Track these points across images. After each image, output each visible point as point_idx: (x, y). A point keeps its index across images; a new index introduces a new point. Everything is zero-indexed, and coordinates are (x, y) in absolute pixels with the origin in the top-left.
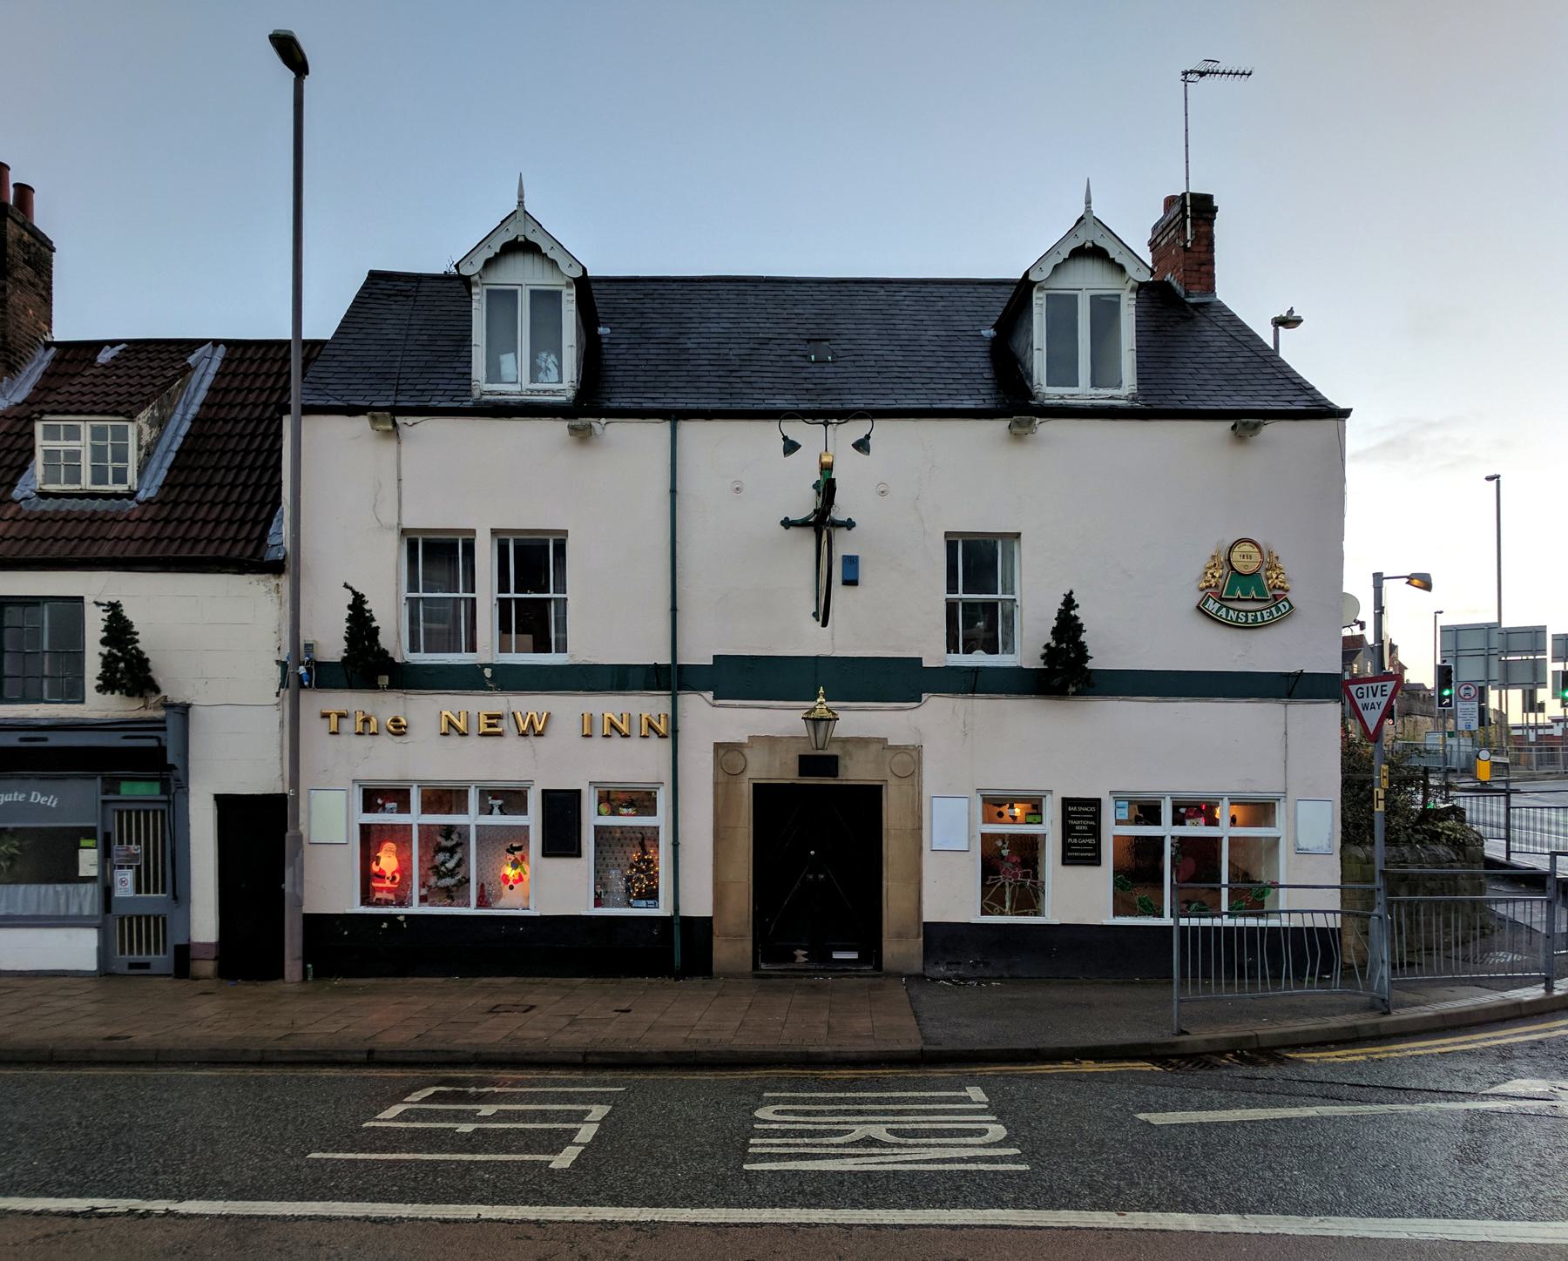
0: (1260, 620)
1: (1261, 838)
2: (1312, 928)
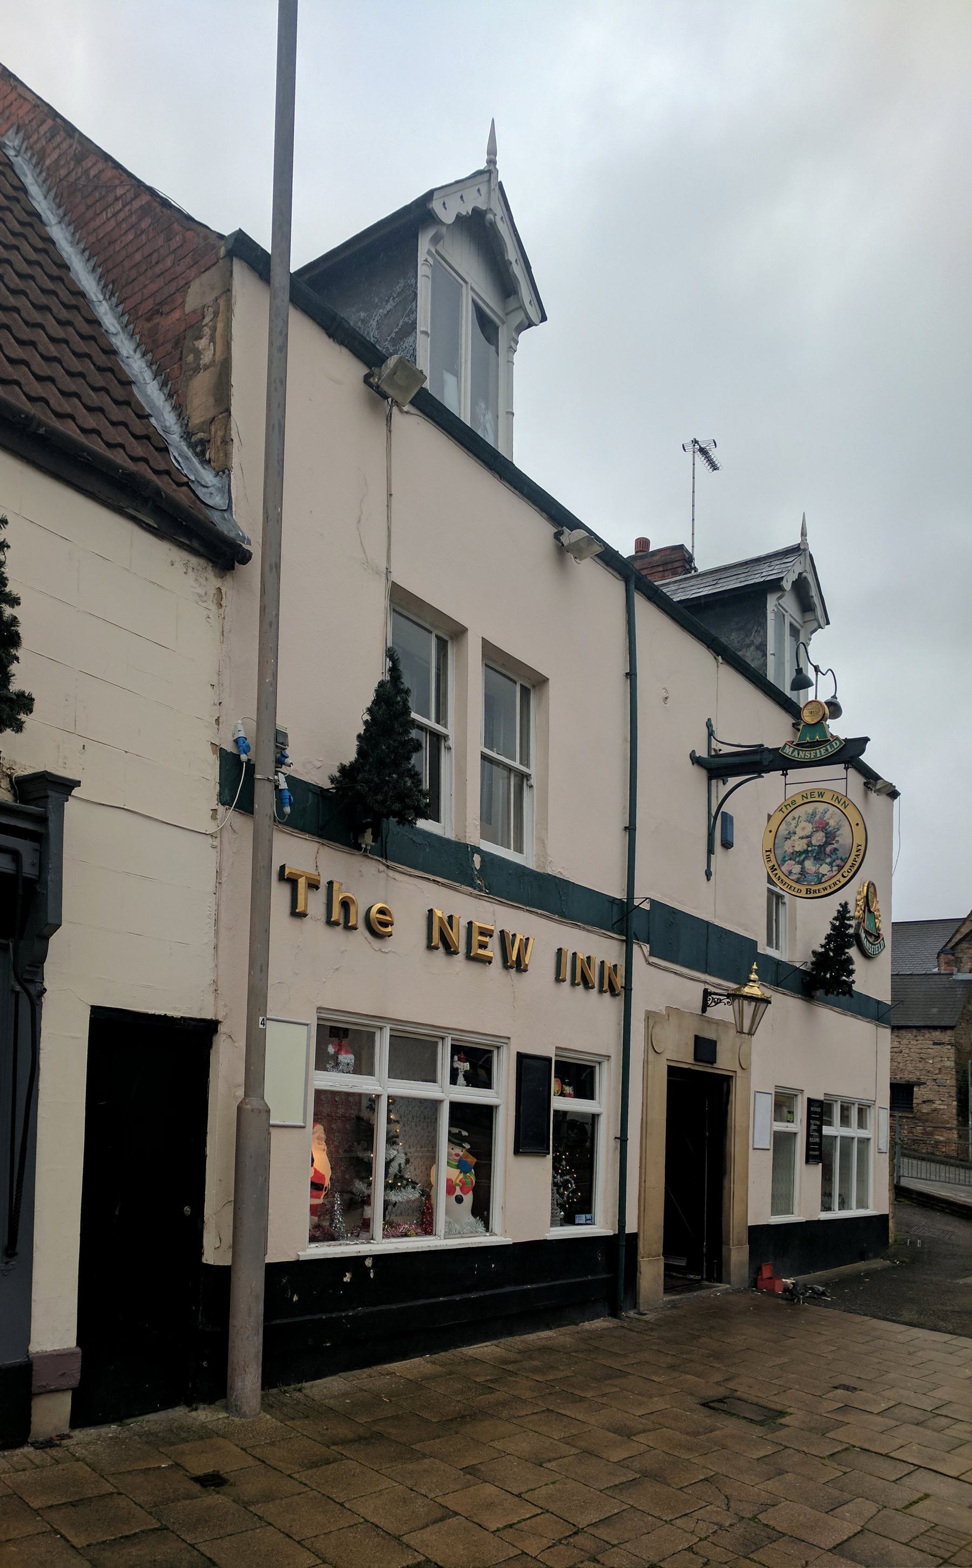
0: (819, 755)
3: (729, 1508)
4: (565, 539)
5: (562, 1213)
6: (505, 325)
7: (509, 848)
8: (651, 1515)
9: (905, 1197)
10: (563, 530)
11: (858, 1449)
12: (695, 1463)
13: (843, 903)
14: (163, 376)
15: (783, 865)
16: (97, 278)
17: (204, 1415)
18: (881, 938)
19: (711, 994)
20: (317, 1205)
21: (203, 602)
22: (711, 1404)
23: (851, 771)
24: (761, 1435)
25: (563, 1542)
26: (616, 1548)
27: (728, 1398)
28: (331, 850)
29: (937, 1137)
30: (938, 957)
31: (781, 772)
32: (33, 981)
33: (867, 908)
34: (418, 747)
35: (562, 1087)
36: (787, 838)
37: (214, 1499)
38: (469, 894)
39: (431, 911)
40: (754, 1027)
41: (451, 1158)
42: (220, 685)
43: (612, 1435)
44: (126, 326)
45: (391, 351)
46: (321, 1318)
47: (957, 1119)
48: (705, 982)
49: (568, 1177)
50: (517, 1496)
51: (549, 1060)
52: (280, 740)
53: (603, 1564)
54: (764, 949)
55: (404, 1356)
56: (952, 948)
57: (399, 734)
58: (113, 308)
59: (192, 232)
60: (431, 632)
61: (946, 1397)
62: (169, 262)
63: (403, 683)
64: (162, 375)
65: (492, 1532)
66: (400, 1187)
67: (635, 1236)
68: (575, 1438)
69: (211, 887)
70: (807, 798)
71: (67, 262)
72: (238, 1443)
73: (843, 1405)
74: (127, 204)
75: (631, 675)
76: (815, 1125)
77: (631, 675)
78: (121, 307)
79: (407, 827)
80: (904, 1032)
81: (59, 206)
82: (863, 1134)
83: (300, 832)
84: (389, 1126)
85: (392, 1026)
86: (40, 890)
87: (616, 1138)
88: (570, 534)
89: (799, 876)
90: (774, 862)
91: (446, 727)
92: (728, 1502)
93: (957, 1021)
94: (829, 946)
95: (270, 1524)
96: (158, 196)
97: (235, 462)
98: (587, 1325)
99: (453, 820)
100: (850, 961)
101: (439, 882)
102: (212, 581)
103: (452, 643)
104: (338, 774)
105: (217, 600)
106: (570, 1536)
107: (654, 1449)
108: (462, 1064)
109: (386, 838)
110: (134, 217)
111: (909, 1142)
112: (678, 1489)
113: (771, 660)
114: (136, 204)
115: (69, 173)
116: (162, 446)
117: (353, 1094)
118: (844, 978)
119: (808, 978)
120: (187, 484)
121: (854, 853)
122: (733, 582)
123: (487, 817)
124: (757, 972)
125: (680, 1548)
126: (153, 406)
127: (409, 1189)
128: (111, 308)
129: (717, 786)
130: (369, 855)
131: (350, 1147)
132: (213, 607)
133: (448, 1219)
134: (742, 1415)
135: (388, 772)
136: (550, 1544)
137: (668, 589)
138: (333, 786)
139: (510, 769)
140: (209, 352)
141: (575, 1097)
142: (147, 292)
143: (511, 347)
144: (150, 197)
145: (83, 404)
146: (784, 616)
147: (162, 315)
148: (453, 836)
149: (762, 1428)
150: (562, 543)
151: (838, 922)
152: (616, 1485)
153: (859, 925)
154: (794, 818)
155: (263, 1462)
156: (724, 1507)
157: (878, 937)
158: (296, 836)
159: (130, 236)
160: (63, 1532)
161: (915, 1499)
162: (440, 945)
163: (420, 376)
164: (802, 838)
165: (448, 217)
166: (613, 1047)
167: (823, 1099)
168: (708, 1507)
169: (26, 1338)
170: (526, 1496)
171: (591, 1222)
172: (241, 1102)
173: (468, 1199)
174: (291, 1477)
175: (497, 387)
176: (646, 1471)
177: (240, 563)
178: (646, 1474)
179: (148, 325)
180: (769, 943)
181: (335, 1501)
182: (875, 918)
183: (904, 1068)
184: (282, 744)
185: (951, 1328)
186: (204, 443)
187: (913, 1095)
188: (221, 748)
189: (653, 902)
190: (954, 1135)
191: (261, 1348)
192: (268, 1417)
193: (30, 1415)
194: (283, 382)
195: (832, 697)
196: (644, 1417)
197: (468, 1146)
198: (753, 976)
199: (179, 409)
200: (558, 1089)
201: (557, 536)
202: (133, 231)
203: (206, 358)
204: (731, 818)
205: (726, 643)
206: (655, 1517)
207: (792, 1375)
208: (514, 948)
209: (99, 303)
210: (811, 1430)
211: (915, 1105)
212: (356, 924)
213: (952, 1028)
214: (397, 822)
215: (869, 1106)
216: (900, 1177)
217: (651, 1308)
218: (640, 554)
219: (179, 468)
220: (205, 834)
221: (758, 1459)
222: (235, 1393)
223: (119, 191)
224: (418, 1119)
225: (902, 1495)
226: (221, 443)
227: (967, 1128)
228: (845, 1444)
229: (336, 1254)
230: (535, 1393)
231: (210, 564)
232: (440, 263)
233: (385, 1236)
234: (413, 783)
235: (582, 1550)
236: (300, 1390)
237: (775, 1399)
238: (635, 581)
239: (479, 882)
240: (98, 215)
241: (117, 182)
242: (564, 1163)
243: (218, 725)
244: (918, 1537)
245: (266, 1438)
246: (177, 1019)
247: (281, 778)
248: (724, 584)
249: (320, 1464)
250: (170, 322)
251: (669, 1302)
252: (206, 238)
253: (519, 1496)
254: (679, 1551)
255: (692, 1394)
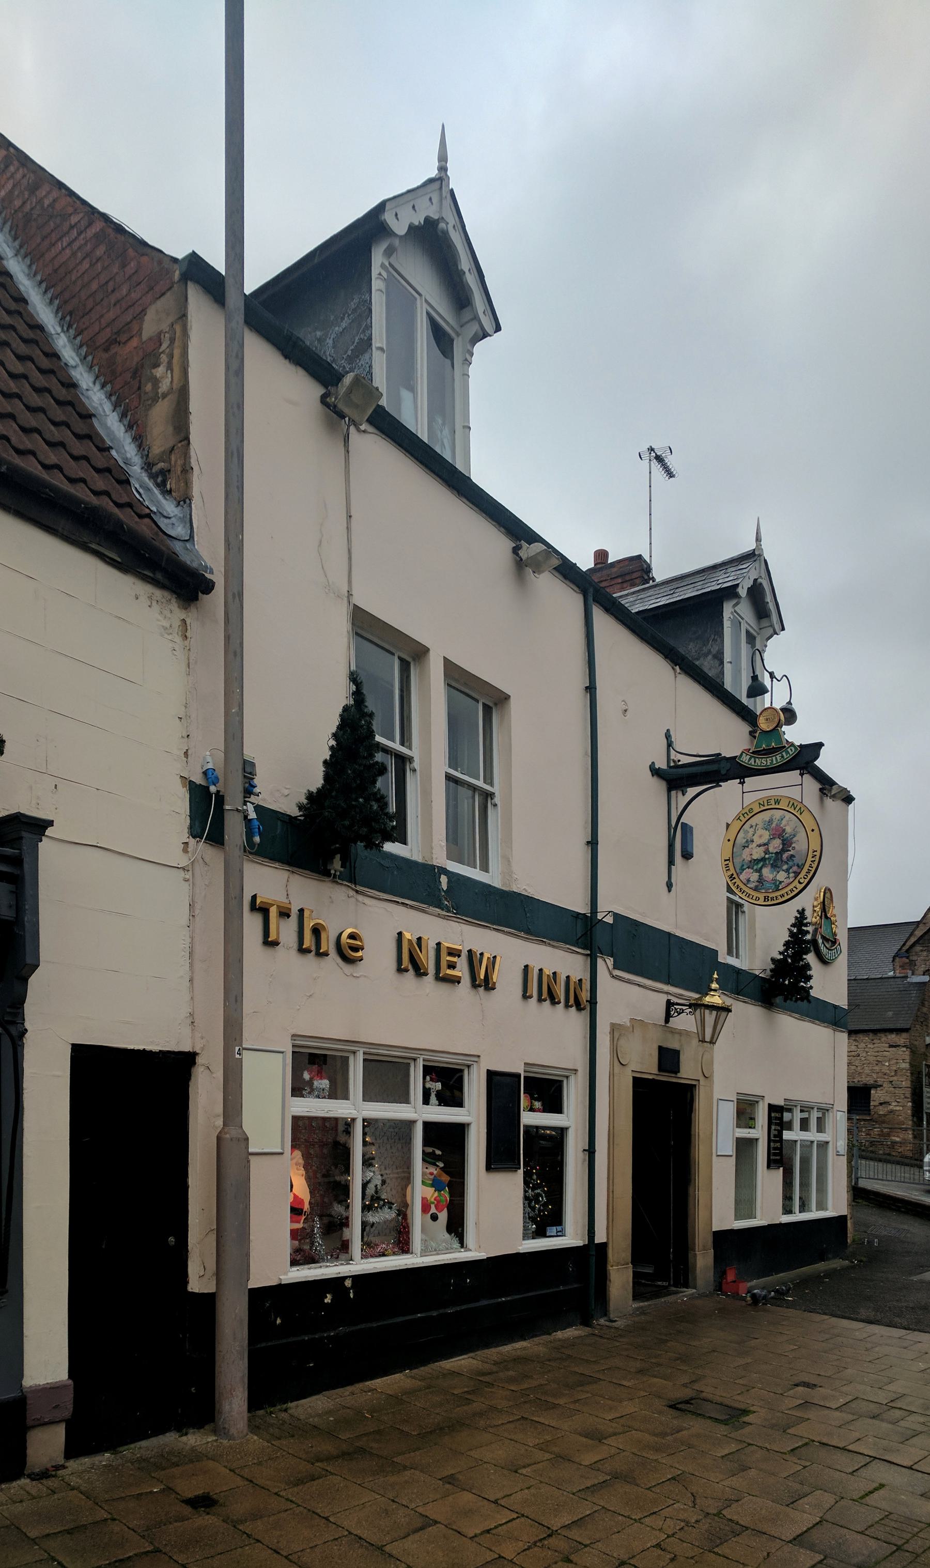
0: (775, 762)
3: (695, 1505)
4: (523, 554)
5: (534, 1226)
6: (460, 338)
7: (475, 868)
8: (622, 1515)
9: (862, 1198)
10: (521, 545)
11: (818, 1444)
12: (663, 1463)
13: (800, 909)
14: (123, 407)
15: (741, 873)
16: (54, 311)
17: (194, 1440)
18: (838, 943)
19: (674, 1004)
20: (298, 1229)
21: (169, 634)
22: (677, 1406)
23: (807, 777)
24: (725, 1433)
25: (538, 1544)
26: (588, 1548)
27: (694, 1399)
28: (303, 878)
29: (893, 1138)
30: (893, 961)
31: (738, 781)
32: (14, 1023)
33: (823, 913)
34: (382, 770)
35: (531, 1103)
36: (744, 847)
37: (206, 1520)
38: (437, 915)
39: (400, 934)
40: (716, 1036)
41: (426, 1177)
42: (188, 717)
43: (584, 1440)
44: (85, 358)
45: (347, 369)
46: (304, 1340)
47: (913, 1120)
48: (667, 993)
49: (539, 1191)
50: (494, 1503)
51: (518, 1076)
52: (248, 769)
53: (576, 1564)
54: (725, 959)
55: (386, 1373)
56: (907, 951)
57: (365, 758)
58: (72, 340)
59: (146, 257)
60: (393, 654)
61: (900, 1390)
62: (125, 290)
63: (366, 707)
64: (121, 406)
65: (471, 1538)
66: (377, 1208)
67: (604, 1246)
68: (548, 1444)
69: (184, 920)
70: (764, 806)
71: (25, 295)
72: (226, 1464)
73: (803, 1402)
74: (81, 232)
75: (591, 689)
76: (775, 1130)
77: (591, 689)
78: (79, 339)
79: (374, 851)
80: (861, 1036)
81: (15, 239)
82: (821, 1137)
83: (271, 861)
84: (365, 1149)
85: (365, 1050)
86: (17, 932)
87: (584, 1150)
88: (528, 548)
89: (758, 884)
90: (732, 871)
91: (410, 749)
92: (695, 1499)
93: (912, 1024)
94: (788, 953)
95: (258, 1541)
96: (112, 222)
97: (196, 491)
98: (559, 1334)
99: (420, 842)
100: (808, 967)
101: (407, 905)
102: (175, 613)
103: (415, 665)
104: (305, 801)
105: (182, 632)
106: (544, 1538)
107: (624, 1451)
108: (434, 1084)
109: (355, 863)
110: (89, 244)
111: (867, 1143)
112: (646, 1489)
113: (728, 668)
114: (90, 232)
115: (24, 203)
116: (124, 478)
117: (330, 1118)
118: (802, 984)
119: (767, 985)
120: (148, 516)
121: (810, 859)
122: (690, 591)
123: (453, 836)
124: (717, 981)
125: (649, 1545)
126: (113, 438)
127: (386, 1209)
128: (69, 341)
129: (677, 797)
130: (339, 881)
131: (328, 1171)
132: (178, 639)
133: (424, 1237)
134: (708, 1415)
135: (354, 796)
136: (526, 1547)
137: (627, 601)
138: (301, 813)
139: (474, 788)
140: (167, 380)
141: (544, 1111)
142: (104, 322)
143: (466, 360)
144: (104, 224)
145: (44, 439)
146: (740, 623)
147: (119, 344)
148: (420, 858)
149: (727, 1427)
150: (520, 557)
151: (796, 929)
152: (588, 1488)
153: (816, 931)
154: (752, 826)
155: (251, 1481)
156: (691, 1504)
157: (834, 942)
158: (266, 865)
159: (86, 265)
160: (60, 1559)
161: (871, 1488)
162: (410, 967)
163: (375, 393)
164: (760, 846)
165: (400, 228)
166: (580, 1062)
167: (783, 1104)
168: (675, 1505)
169: (21, 1375)
170: (502, 1502)
171: (561, 1234)
172: (220, 1132)
173: (443, 1216)
174: (279, 1495)
175: (454, 407)
176: (617, 1472)
177: (203, 593)
178: (616, 1476)
179: (105, 356)
180: (730, 952)
181: (320, 1516)
182: (832, 923)
183: (861, 1071)
184: (250, 773)
185: (906, 1323)
186: (165, 473)
187: (870, 1098)
188: (190, 781)
189: (616, 916)
190: (910, 1136)
191: (246, 1372)
192: (256, 1438)
193: (25, 1448)
194: (240, 406)
195: (787, 703)
196: (614, 1421)
197: (441, 1165)
198: (714, 985)
199: (139, 440)
200: (527, 1104)
201: (515, 551)
202: (88, 260)
203: (164, 386)
204: (691, 829)
205: (684, 653)
206: (625, 1517)
207: (755, 1375)
208: (482, 967)
209: (57, 336)
210: (773, 1427)
211: (872, 1107)
212: (327, 951)
213: (906, 1030)
214: (364, 846)
215: (828, 1110)
216: (857, 1179)
217: (620, 1315)
218: (599, 566)
219: (141, 499)
220: (178, 868)
221: (723, 1457)
222: (223, 1417)
223: (74, 219)
224: (393, 1141)
225: (859, 1485)
226: (182, 472)
227: (920, 1128)
228: (805, 1439)
229: (316, 1276)
230: (510, 1403)
231: (174, 596)
232: (395, 276)
233: (364, 1257)
234: (379, 806)
235: (556, 1551)
236: (286, 1410)
237: (739, 1398)
238: (593, 594)
239: (446, 903)
240: (54, 245)
241: (70, 210)
242: (535, 1177)
243: (187, 758)
244: (872, 1526)
245: (254, 1459)
246: (155, 1053)
247: (250, 808)
248: (681, 593)
249: (305, 1481)
250: (128, 352)
251: (638, 1309)
252: (160, 262)
253: (496, 1502)
254: (648, 1548)
255: (659, 1397)
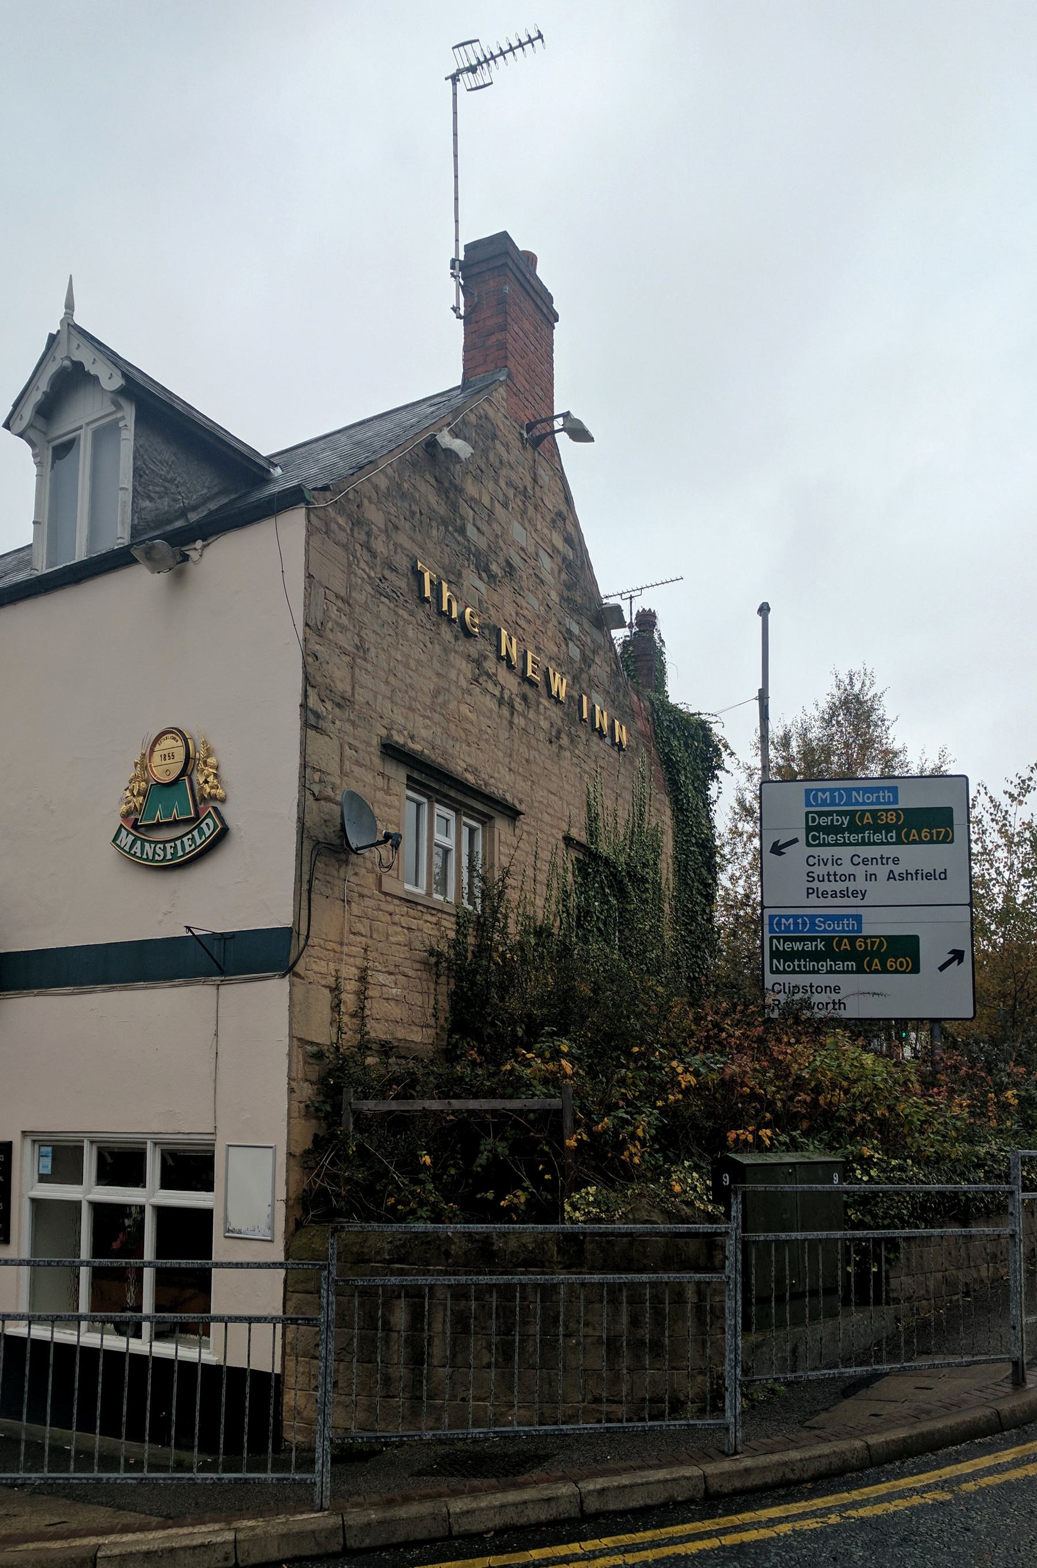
1: (130, 1206)
2: (242, 1370)
